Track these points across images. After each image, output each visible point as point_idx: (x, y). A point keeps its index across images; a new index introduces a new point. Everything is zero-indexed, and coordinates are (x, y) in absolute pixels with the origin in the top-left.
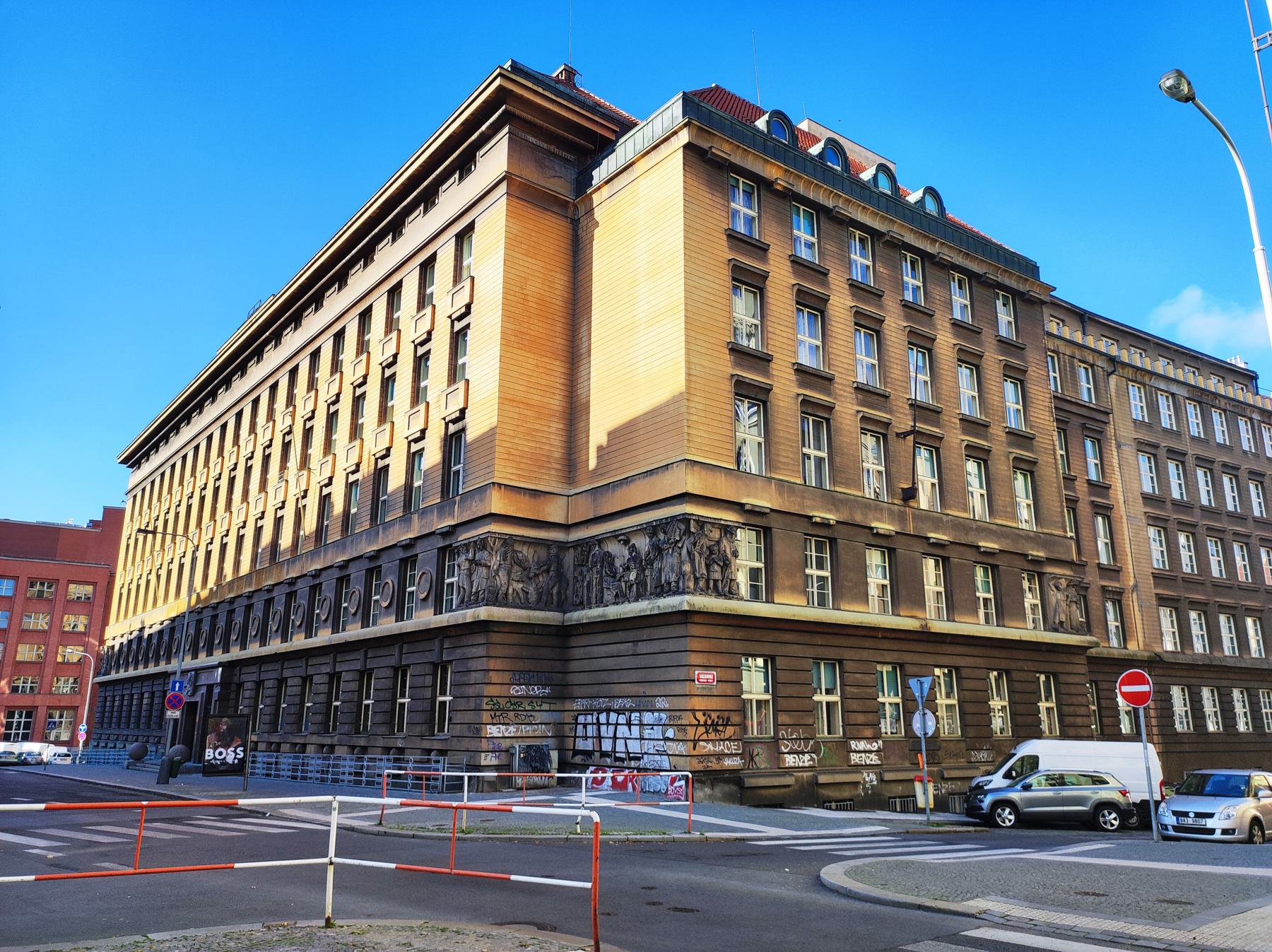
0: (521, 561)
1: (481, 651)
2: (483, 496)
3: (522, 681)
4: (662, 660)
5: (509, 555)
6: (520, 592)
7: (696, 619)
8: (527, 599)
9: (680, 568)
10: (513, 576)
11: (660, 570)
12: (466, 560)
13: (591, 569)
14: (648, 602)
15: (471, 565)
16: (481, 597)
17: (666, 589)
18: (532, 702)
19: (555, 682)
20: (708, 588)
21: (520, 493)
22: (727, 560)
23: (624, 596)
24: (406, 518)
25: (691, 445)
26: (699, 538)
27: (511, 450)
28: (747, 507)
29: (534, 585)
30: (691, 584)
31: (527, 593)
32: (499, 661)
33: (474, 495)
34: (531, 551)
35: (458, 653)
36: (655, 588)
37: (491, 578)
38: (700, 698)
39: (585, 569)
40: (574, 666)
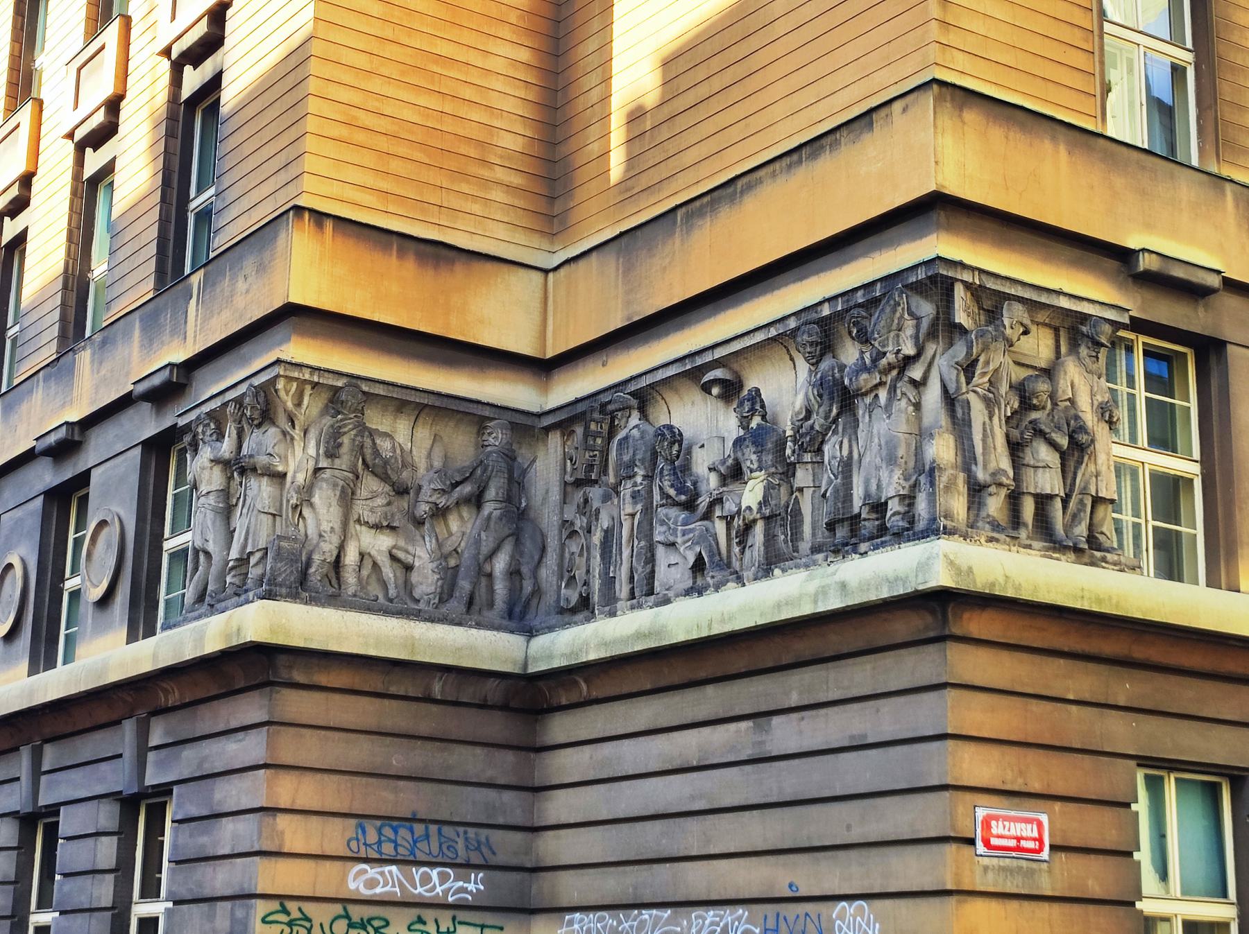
0: (386, 462)
1: (249, 748)
2: (267, 255)
3: (388, 849)
4: (1036, 45)
5: (346, 440)
6: (384, 561)
7: (977, 624)
8: (408, 587)
9: (919, 452)
10: (361, 508)
11: (847, 467)
12: (216, 461)
13: (616, 489)
14: (802, 575)
15: (230, 478)
16: (254, 573)
17: (869, 526)
18: (421, 921)
19: (501, 859)
20: (1016, 521)
21: (386, 248)
22: (1082, 429)
23: (725, 565)
24: (59, 367)
25: (953, 38)
26: (985, 348)
27: (361, 114)
28: (1146, 263)
29: (430, 543)
30: (958, 505)
31: (408, 568)
32: (309, 781)
33: (241, 258)
34: (424, 434)
35: (188, 761)
36: (831, 526)
37: (287, 511)
38: (994, 906)
39: (595, 493)
40: (560, 806)
